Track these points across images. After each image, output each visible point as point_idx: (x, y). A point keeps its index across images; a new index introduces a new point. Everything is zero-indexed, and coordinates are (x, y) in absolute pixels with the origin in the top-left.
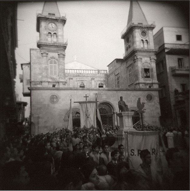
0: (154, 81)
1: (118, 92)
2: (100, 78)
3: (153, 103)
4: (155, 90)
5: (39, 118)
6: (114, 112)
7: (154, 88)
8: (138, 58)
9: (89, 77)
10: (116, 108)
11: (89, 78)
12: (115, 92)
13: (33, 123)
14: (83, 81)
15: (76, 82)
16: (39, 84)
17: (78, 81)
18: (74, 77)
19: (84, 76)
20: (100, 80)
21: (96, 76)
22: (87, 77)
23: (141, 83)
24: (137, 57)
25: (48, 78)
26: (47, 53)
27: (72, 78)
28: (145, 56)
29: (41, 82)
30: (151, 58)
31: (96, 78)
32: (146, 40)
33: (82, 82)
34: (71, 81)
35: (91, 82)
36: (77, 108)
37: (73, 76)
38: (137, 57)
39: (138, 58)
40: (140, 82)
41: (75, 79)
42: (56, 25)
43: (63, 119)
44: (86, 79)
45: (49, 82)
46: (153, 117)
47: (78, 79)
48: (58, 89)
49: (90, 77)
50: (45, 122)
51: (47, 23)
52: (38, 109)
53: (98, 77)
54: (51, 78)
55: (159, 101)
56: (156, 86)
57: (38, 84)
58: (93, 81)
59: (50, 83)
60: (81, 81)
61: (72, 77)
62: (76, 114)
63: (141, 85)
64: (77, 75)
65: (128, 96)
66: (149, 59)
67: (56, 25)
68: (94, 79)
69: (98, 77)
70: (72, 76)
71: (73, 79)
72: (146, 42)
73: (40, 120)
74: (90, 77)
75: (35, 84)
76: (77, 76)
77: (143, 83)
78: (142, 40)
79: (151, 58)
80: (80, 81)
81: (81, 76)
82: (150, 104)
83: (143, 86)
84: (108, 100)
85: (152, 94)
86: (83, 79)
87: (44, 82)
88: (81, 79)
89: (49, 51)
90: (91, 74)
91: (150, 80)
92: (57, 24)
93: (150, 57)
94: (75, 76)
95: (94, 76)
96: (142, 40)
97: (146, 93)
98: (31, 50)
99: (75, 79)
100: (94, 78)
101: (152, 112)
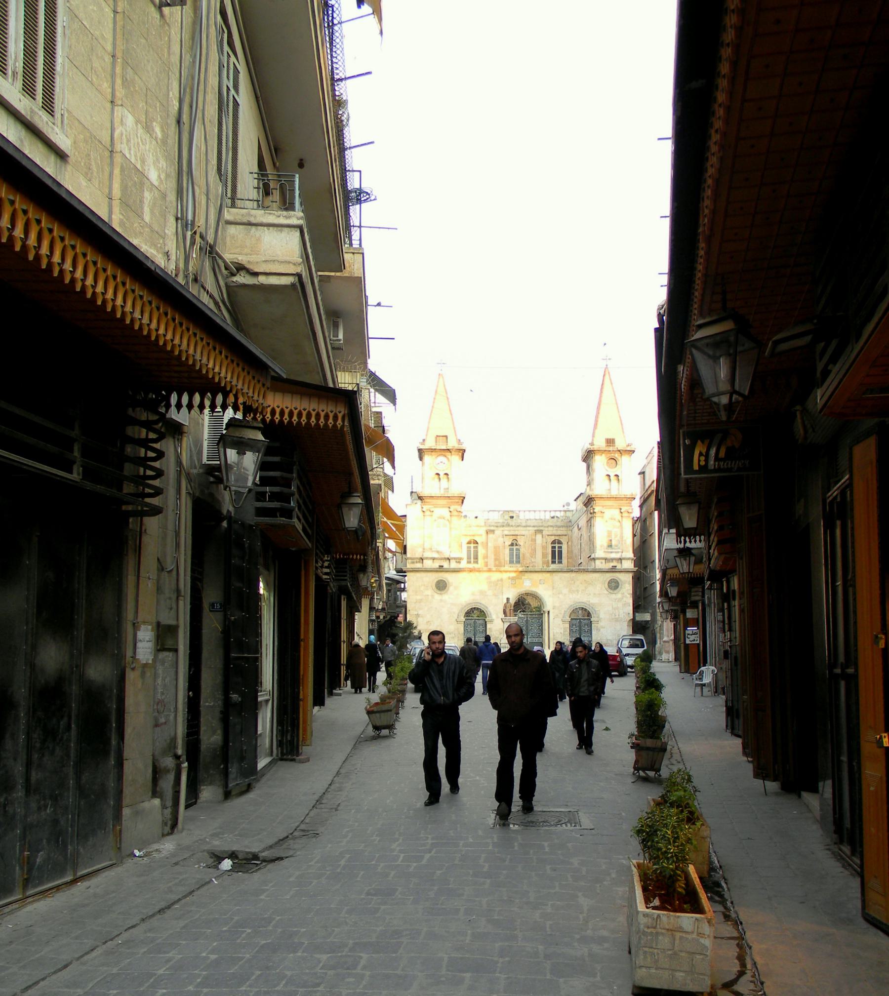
0: (625, 555)
1: (554, 574)
2: (555, 529)
3: (619, 596)
4: (626, 571)
5: (418, 615)
6: (544, 610)
7: (623, 567)
8: (595, 511)
9: (529, 526)
10: (547, 604)
11: (530, 528)
12: (548, 575)
13: (230, 465)
14: (517, 535)
15: (502, 539)
16: (419, 562)
17: (506, 535)
18: (497, 527)
19: (518, 526)
20: (555, 532)
21: (546, 525)
22: (526, 526)
23: (599, 559)
24: (594, 509)
25: (433, 551)
26: (432, 510)
27: (493, 531)
28: (611, 507)
29: (422, 559)
30: (622, 511)
31: (546, 529)
32: (617, 476)
33: (514, 537)
34: (491, 536)
35: (534, 537)
36: (479, 601)
37: (496, 525)
38: (594, 509)
39: (595, 511)
40: (597, 556)
41: (498, 532)
42: (448, 459)
43: (454, 620)
44: (523, 533)
45: (434, 559)
46: (617, 620)
47: (506, 533)
48: (447, 571)
49: (534, 527)
50: (428, 622)
51: (434, 457)
52: (416, 602)
53: (551, 526)
54: (438, 552)
55: (631, 592)
56: (629, 565)
57: (417, 562)
58: (539, 537)
59: (435, 560)
60: (513, 535)
61: (492, 528)
62: (135, 667)
63: (597, 562)
64: (504, 523)
65: (573, 582)
66: (618, 511)
67: (448, 459)
68: (541, 531)
69: (551, 526)
70: (493, 526)
71: (496, 532)
72: (616, 478)
73: (420, 620)
74: (534, 527)
75: (413, 563)
76: (503, 526)
77: (602, 559)
78: (608, 475)
79: (622, 511)
80: (511, 537)
81: (512, 526)
82: (613, 596)
83: (602, 563)
84: (533, 589)
85: (619, 578)
86: (516, 533)
87: (427, 558)
88: (513, 533)
89: (436, 506)
90: (534, 521)
91: (618, 552)
92: (449, 457)
93: (621, 509)
94: (499, 525)
95: (541, 524)
96: (608, 475)
97: (609, 576)
98: (446, 436)
99: (498, 532)
100: (541, 528)
101: (617, 611)
